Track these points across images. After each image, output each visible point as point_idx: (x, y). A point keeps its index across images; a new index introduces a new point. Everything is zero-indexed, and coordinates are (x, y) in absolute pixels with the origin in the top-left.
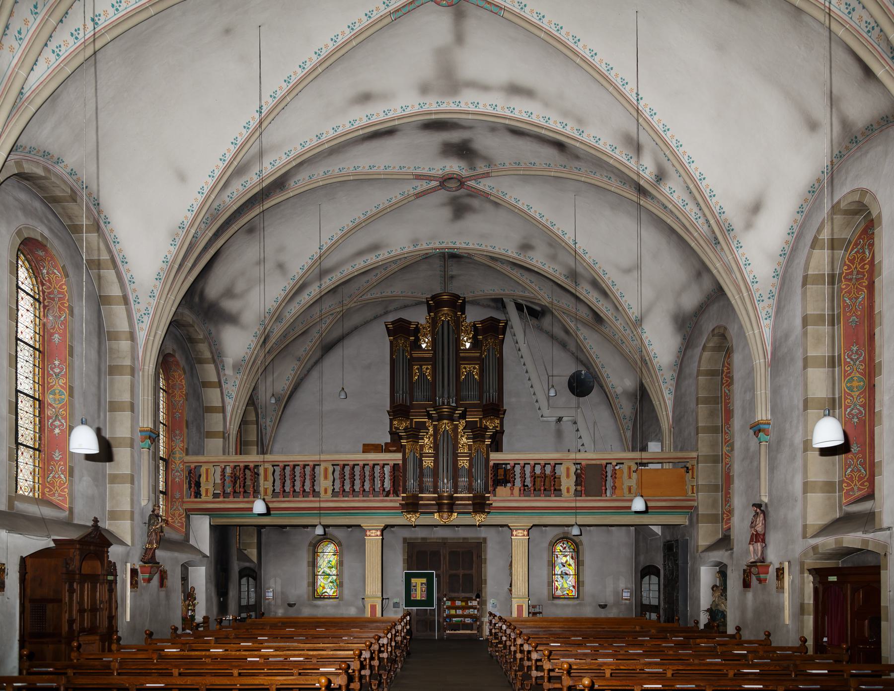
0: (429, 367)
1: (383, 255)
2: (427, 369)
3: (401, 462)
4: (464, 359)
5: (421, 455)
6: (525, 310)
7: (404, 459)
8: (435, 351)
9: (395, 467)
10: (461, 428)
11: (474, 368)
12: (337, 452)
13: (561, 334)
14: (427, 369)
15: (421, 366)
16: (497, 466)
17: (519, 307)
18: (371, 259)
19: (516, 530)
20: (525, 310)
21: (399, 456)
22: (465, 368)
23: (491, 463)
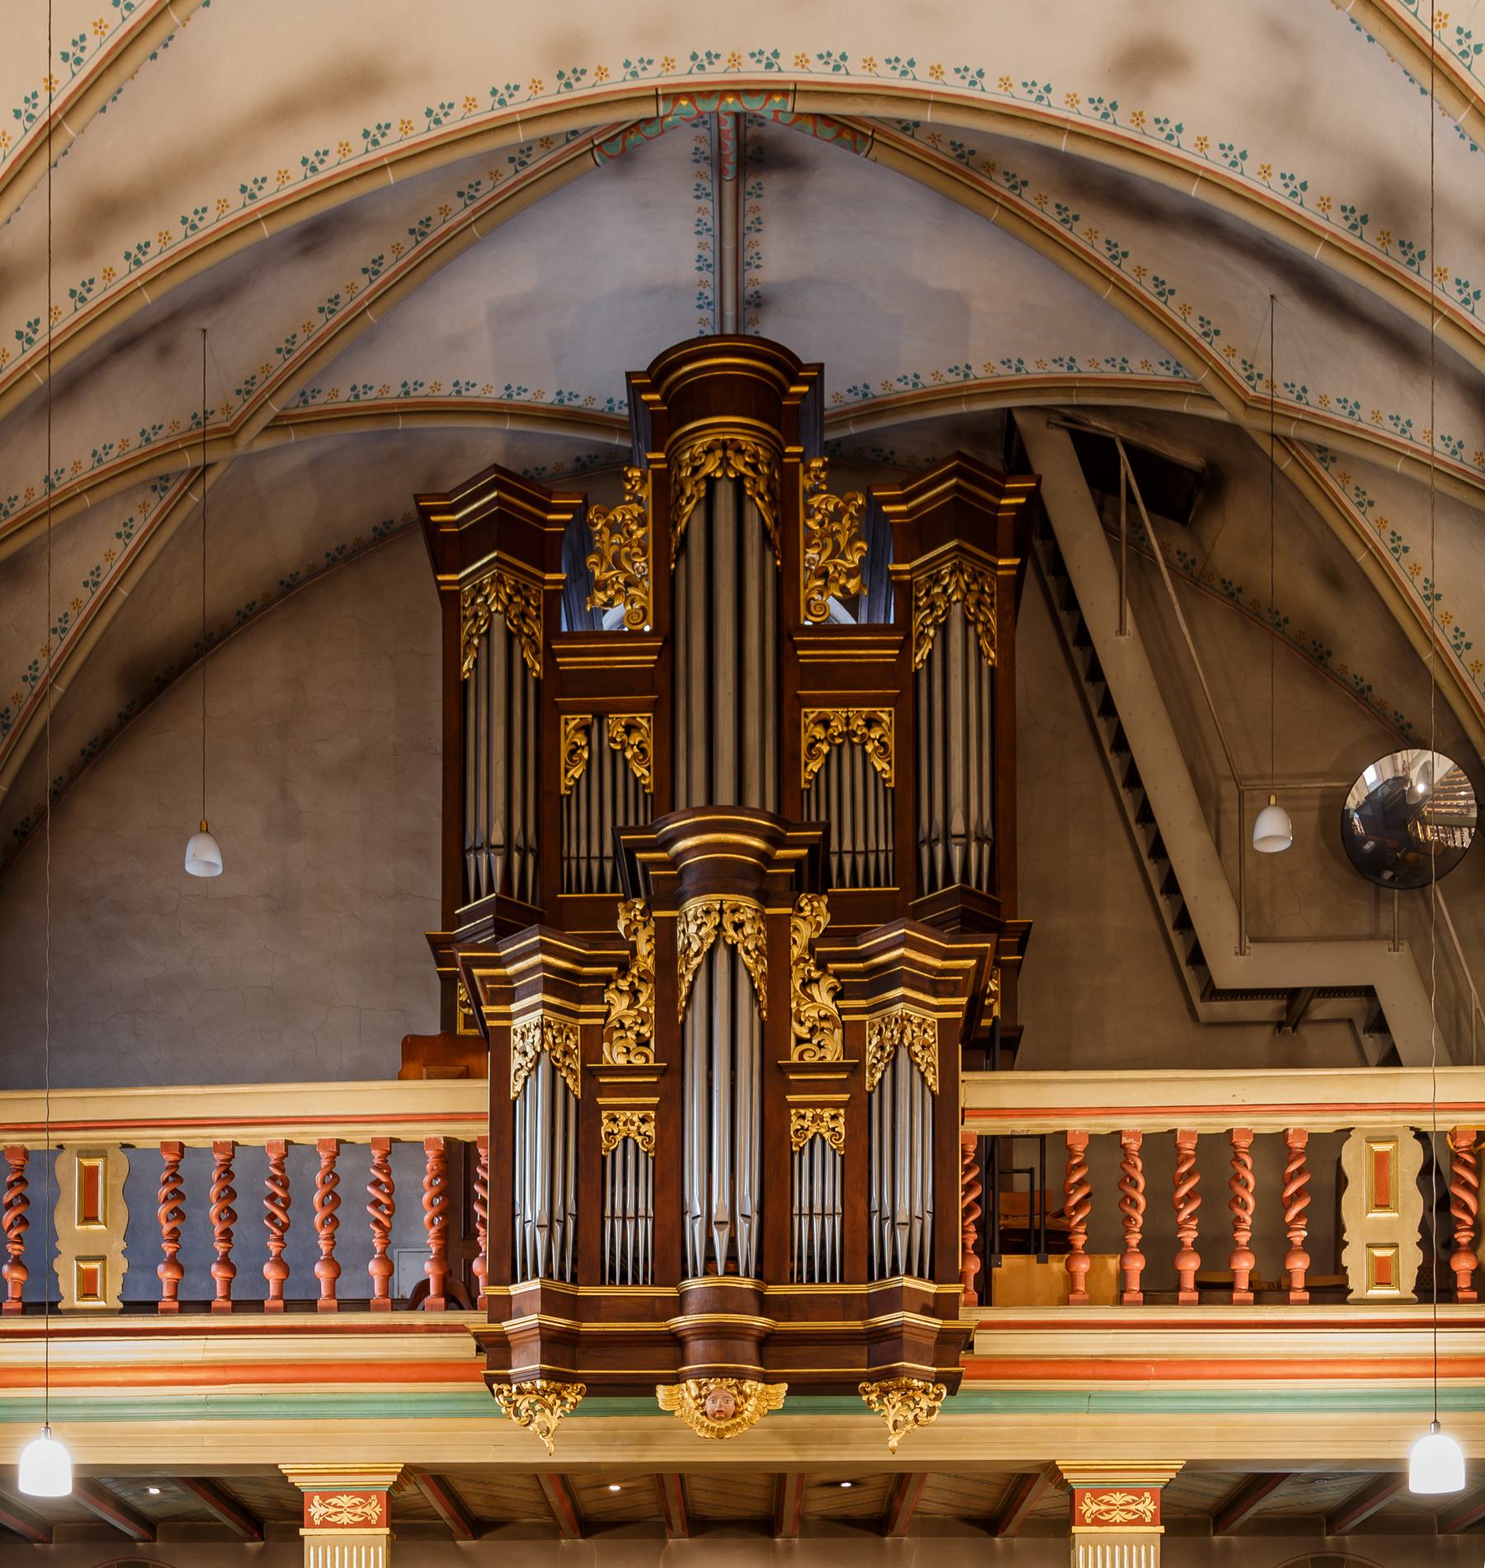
0: (642, 719)
1: (404, 120)
2: (630, 729)
3: (482, 1129)
4: (823, 675)
5: (589, 1075)
6: (1125, 468)
7: (503, 1113)
8: (670, 641)
9: (457, 1160)
10: (803, 933)
11: (871, 722)
12: (203, 1431)
13: (1304, 592)
14: (630, 729)
15: (600, 717)
16: (994, 1150)
17: (1096, 459)
18: (338, 143)
19: (1097, 1494)
20: (1125, 468)
21: (474, 1095)
22: (825, 723)
23: (972, 1128)
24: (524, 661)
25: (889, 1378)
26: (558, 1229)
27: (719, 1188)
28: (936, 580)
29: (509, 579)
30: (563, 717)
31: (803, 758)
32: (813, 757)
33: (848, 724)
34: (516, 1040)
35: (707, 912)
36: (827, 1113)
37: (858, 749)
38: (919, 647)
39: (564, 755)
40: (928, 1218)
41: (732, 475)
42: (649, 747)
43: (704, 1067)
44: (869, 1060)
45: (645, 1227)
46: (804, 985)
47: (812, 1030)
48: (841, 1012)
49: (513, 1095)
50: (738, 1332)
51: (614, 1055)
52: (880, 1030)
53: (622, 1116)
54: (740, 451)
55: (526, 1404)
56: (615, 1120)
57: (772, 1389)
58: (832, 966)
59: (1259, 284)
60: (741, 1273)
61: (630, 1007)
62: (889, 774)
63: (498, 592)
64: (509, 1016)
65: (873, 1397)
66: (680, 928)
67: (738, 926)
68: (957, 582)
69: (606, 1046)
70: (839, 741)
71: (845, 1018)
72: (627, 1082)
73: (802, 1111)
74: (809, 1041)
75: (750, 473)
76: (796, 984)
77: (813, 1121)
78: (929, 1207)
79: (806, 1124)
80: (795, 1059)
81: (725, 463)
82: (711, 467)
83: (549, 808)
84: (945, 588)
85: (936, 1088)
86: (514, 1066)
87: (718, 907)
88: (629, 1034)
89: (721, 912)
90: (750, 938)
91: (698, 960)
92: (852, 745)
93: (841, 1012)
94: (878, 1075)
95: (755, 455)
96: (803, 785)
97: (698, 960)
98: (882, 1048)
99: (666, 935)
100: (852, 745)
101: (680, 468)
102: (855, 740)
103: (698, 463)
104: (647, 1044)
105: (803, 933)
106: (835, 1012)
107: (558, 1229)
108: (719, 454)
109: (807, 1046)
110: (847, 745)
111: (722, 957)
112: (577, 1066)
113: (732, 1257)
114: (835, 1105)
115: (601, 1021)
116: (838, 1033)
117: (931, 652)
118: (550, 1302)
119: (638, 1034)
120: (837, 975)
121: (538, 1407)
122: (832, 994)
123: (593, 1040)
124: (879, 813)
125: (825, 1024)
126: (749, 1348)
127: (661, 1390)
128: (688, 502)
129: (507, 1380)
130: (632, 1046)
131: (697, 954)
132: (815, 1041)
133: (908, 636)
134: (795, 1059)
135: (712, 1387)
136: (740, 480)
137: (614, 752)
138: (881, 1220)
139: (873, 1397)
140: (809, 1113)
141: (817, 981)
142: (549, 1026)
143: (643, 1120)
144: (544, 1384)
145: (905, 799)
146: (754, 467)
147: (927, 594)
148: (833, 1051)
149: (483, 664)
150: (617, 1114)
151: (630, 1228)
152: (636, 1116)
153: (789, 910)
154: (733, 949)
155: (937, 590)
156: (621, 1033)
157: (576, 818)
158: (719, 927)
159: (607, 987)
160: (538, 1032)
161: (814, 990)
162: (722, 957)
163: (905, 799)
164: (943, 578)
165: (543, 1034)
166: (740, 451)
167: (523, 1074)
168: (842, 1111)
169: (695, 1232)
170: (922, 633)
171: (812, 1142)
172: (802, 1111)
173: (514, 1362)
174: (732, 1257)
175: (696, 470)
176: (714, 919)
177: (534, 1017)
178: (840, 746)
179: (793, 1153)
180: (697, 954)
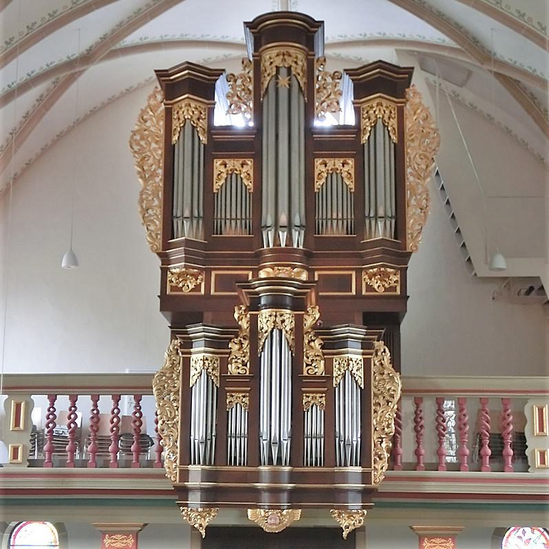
10: (309, 322)
24: (199, 137)
25: (343, 509)
26: (209, 442)
27: (275, 423)
28: (372, 107)
29: (193, 105)
30: (215, 160)
31: (316, 180)
32: (320, 179)
33: (334, 165)
34: (192, 363)
35: (270, 316)
36: (318, 395)
37: (339, 175)
38: (364, 134)
39: (215, 176)
40: (359, 440)
41: (286, 66)
42: (251, 173)
43: (292, 135)
44: (335, 375)
45: (244, 441)
46: (309, 342)
47: (312, 361)
48: (324, 354)
49: (191, 386)
50: (281, 490)
51: (233, 369)
52: (339, 363)
53: (236, 395)
54: (290, 56)
55: (194, 515)
56: (232, 396)
57: (295, 511)
58: (320, 337)
59: (411, 375)
60: (284, 464)
61: (239, 350)
62: (352, 186)
63: (188, 110)
64: (190, 353)
65: (336, 515)
66: (259, 319)
67: (283, 321)
68: (380, 110)
69: (229, 366)
70: (331, 172)
71: (325, 357)
72: (238, 381)
73: (308, 395)
74: (311, 365)
75: (294, 65)
76: (306, 341)
77: (312, 399)
78: (359, 436)
79: (309, 399)
80: (305, 374)
81: (284, 60)
82: (278, 62)
83: (210, 199)
84: (375, 112)
85: (362, 386)
86: (192, 374)
87: (274, 314)
88: (239, 361)
89: (276, 316)
90: (289, 324)
91: (266, 335)
92: (337, 173)
93: (324, 354)
94: (338, 381)
95: (297, 58)
96: (316, 190)
97: (266, 335)
98: (340, 370)
99: (254, 321)
100: (337, 173)
101: (265, 61)
102: (338, 172)
103: (272, 60)
104: (246, 365)
105: (309, 322)
106: (321, 354)
107: (209, 442)
108: (281, 57)
109: (310, 367)
110: (334, 173)
111: (276, 333)
112: (218, 374)
113: (279, 459)
114: (322, 393)
115: (228, 356)
116: (322, 362)
117: (369, 137)
118: (208, 476)
119: (243, 361)
120: (322, 339)
121: (199, 517)
122: (320, 346)
123: (224, 364)
124: (348, 203)
125: (317, 358)
126: (285, 496)
127: (250, 511)
128: (268, 75)
129: (186, 505)
130: (240, 366)
131: (266, 332)
132: (313, 365)
133: (360, 129)
134: (305, 374)
135: (270, 513)
136: (289, 69)
137: (237, 175)
138: (339, 441)
139: (336, 515)
140: (311, 395)
141: (314, 341)
142: (207, 359)
143: (244, 397)
144: (202, 510)
145: (359, 198)
146: (296, 63)
147: (367, 112)
148: (320, 369)
149: (181, 137)
150: (233, 394)
151: (238, 446)
152: (241, 395)
153: (303, 312)
154: (281, 331)
155: (372, 112)
156: (236, 360)
157: (220, 203)
158: (275, 322)
159: (230, 341)
160: (202, 362)
161: (312, 344)
162: (276, 333)
163: (359, 198)
164: (373, 107)
165: (204, 363)
166: (290, 56)
167: (195, 377)
168: (324, 395)
169: (264, 443)
170: (365, 128)
171: (312, 407)
172: (308, 395)
173: (189, 499)
174: (279, 459)
175: (271, 63)
176: (273, 318)
177: (201, 356)
178: (332, 174)
179: (304, 412)
180: (266, 332)
